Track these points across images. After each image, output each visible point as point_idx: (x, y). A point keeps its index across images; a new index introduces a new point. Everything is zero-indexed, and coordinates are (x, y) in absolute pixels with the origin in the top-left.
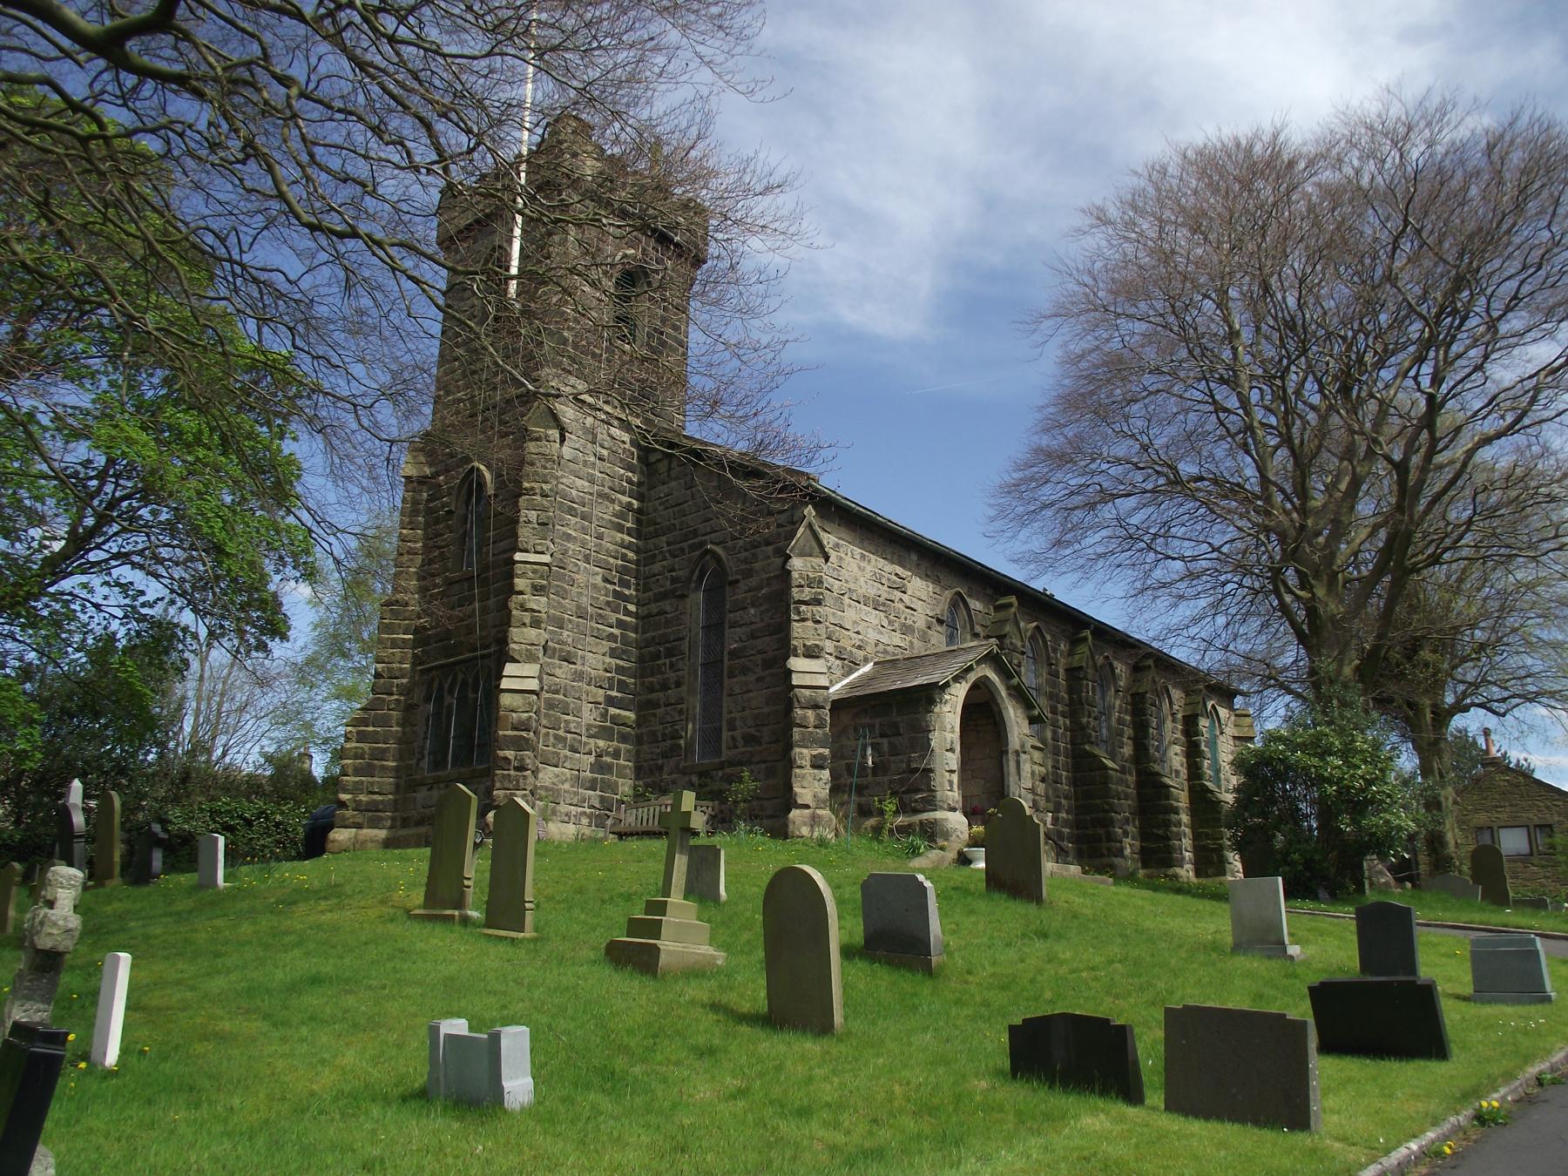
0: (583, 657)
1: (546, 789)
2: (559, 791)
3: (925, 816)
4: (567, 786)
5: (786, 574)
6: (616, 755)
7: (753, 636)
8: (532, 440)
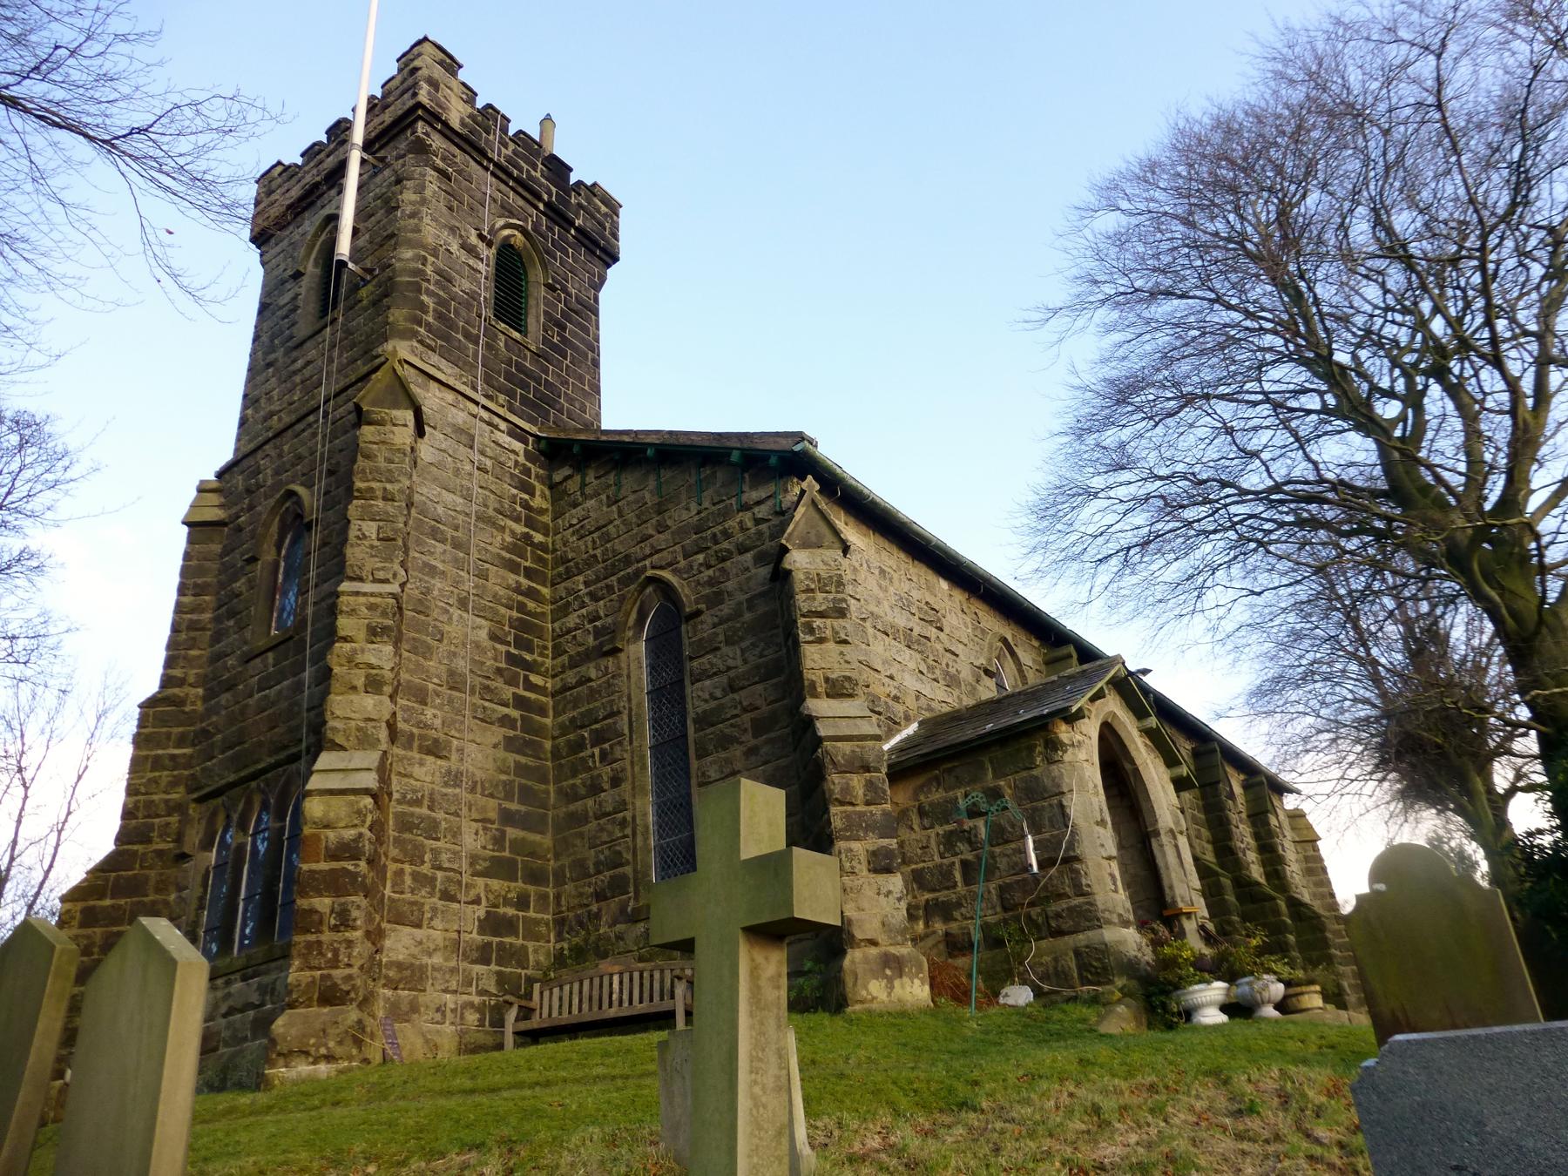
0: (460, 750)
1: (400, 966)
2: (422, 969)
3: (1081, 939)
4: (437, 959)
5: (782, 577)
6: (522, 903)
7: (732, 688)
8: (370, 424)
